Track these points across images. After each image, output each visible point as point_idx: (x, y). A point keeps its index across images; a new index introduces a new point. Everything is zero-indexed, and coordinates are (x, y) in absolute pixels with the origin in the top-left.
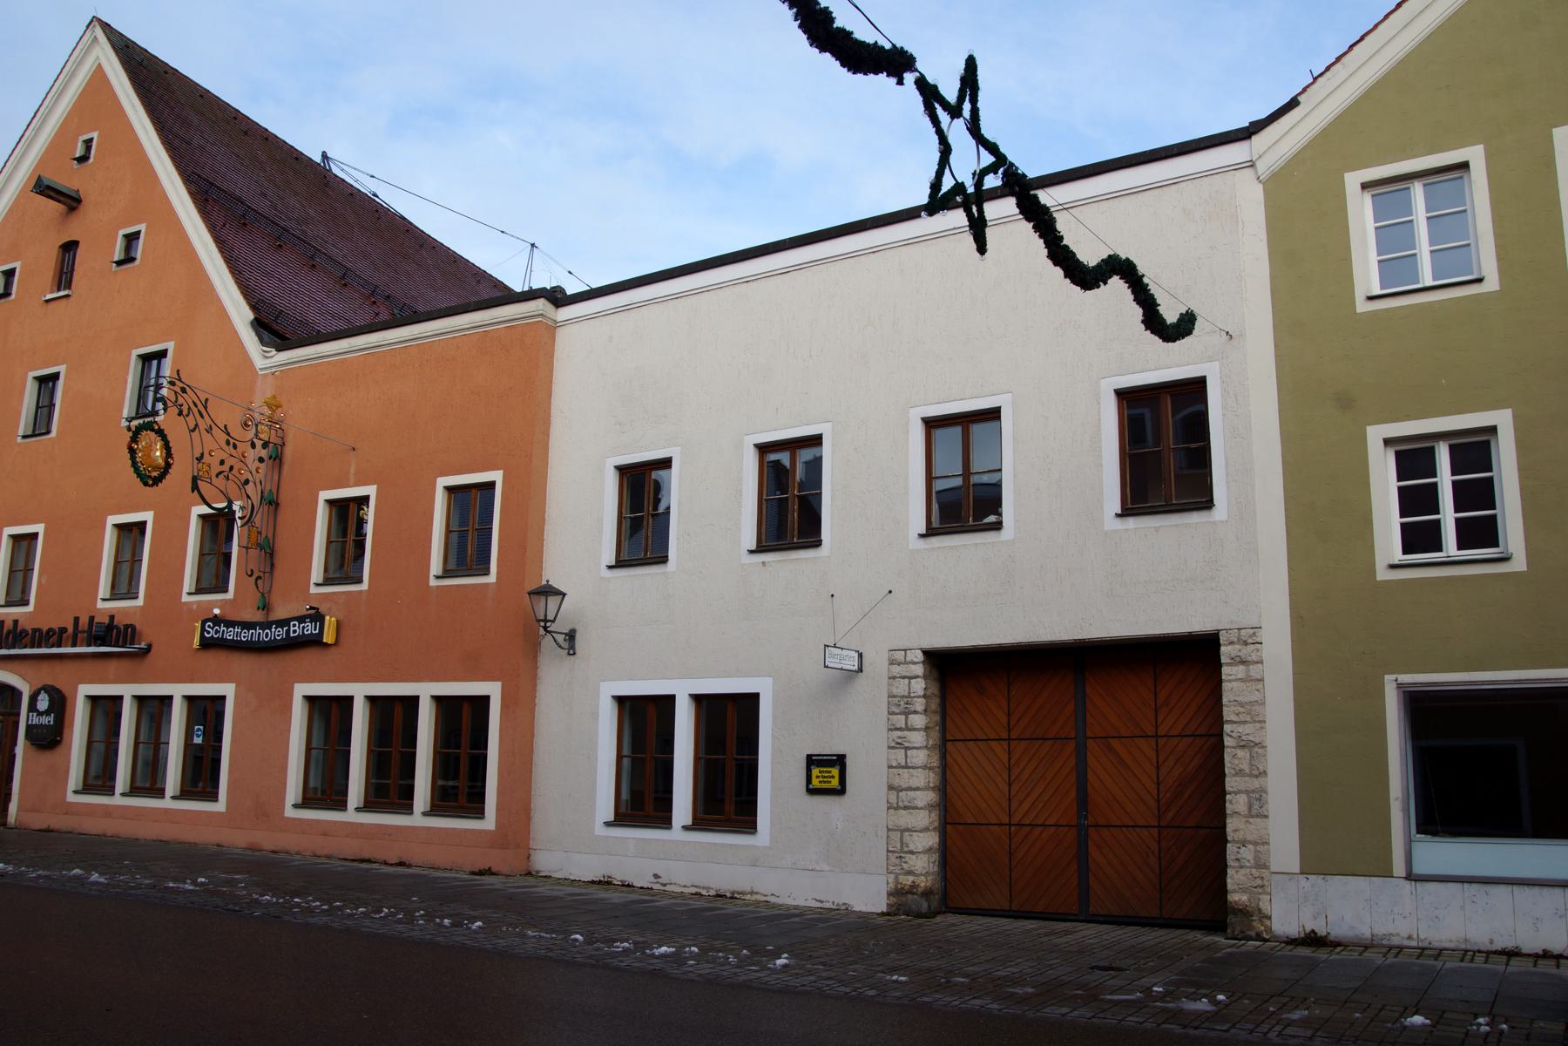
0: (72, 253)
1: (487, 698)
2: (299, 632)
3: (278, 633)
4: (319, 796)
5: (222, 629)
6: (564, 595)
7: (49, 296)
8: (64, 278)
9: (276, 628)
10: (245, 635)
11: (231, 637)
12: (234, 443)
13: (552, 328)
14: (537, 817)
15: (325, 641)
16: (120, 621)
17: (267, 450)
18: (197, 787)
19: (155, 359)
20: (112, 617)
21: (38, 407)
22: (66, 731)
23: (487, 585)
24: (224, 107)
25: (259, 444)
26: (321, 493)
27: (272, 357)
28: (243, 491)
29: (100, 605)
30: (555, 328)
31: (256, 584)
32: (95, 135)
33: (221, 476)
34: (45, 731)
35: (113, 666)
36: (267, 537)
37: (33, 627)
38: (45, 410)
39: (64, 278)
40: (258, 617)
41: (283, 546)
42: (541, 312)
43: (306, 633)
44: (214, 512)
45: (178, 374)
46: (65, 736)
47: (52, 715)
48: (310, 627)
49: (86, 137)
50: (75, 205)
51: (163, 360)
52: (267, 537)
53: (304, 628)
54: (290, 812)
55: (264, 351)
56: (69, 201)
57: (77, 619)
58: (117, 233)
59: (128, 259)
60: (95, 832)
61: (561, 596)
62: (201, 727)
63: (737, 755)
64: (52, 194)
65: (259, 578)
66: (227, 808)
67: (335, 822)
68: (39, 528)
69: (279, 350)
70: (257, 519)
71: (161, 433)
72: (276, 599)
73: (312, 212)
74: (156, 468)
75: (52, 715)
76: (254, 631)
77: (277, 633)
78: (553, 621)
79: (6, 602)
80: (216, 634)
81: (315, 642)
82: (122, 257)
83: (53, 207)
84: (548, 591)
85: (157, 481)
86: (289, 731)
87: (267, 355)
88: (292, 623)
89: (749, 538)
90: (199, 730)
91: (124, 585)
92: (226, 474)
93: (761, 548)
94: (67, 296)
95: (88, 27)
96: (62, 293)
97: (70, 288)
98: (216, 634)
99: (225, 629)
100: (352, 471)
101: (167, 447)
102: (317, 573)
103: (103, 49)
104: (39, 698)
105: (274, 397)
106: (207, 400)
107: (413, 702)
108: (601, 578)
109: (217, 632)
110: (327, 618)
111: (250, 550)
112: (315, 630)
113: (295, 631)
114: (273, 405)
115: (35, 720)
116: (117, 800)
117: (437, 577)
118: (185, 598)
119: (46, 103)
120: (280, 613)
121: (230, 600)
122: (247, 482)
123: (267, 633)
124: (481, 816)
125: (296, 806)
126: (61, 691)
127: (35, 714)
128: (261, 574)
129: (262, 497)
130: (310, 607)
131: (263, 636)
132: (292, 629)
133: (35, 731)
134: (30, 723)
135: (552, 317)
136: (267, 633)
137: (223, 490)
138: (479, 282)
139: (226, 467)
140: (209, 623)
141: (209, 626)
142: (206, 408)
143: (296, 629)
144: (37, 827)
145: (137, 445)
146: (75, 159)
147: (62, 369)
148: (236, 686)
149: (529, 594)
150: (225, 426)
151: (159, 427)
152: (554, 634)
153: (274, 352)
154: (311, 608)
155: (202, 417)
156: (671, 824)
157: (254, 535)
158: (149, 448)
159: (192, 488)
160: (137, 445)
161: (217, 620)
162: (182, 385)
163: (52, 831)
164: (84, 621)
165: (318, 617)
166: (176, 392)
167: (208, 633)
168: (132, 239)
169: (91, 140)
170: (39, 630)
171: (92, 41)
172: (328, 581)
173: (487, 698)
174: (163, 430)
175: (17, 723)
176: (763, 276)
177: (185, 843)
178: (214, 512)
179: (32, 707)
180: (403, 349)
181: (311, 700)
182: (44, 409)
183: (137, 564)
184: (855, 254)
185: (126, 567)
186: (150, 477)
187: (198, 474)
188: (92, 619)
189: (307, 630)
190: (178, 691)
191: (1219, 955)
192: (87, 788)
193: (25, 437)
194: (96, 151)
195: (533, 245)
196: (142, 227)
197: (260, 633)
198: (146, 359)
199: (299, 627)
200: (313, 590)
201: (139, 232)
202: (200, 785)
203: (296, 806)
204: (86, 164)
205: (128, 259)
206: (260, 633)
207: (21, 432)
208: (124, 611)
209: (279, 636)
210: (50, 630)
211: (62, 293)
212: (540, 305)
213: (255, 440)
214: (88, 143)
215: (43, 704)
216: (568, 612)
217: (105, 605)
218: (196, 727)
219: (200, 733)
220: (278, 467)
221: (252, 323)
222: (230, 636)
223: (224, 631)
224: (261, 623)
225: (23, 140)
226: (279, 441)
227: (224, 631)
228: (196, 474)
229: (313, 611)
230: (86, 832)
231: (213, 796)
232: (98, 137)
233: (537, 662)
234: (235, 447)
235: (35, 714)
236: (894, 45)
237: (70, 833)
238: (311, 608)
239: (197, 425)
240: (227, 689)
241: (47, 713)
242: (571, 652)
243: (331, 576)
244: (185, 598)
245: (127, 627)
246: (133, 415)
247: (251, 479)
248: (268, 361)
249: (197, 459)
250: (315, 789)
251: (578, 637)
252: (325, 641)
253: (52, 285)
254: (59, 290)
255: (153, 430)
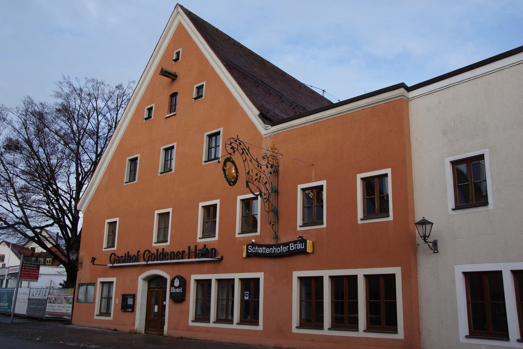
0: (174, 98)
1: (259, 279)
2: (294, 248)
3: (285, 249)
4: (305, 322)
5: (256, 248)
6: (432, 224)
7: (167, 116)
8: (172, 107)
9: (283, 247)
10: (268, 251)
11: (261, 252)
12: (260, 166)
13: (408, 100)
14: (424, 333)
15: (307, 251)
16: (209, 247)
17: (272, 168)
18: (247, 319)
19: (169, 150)
20: (205, 245)
21: (130, 171)
22: (187, 295)
23: (323, 228)
24: (225, 35)
25: (269, 166)
26: (200, 203)
27: (269, 129)
28: (265, 187)
29: (154, 245)
30: (408, 101)
31: (272, 228)
32: (181, 50)
33: (256, 181)
34: (178, 295)
35: (206, 267)
36: (275, 207)
37: (211, 248)
38: (133, 172)
39: (172, 107)
40: (273, 242)
41: (283, 209)
42: (403, 94)
43: (298, 248)
44: (255, 196)
45: (238, 137)
46: (186, 297)
47: (181, 288)
48: (299, 246)
49: (177, 51)
50: (175, 78)
51: (173, 150)
52: (275, 207)
53: (296, 246)
54: (294, 330)
55: (266, 127)
56: (173, 77)
57: (189, 247)
58: (194, 87)
59: (199, 96)
60: (202, 339)
61: (431, 224)
62: (248, 292)
63: (385, 300)
64: (167, 74)
65: (273, 225)
66: (263, 328)
67: (318, 335)
68: (170, 210)
69: (272, 126)
70: (271, 199)
71: (233, 162)
72: (280, 234)
73: (263, 74)
74: (233, 177)
75: (181, 288)
76: (272, 249)
77: (283, 249)
78: (428, 237)
79: (158, 241)
80: (254, 251)
81: (303, 252)
82: (196, 96)
83: (167, 80)
84: (424, 222)
85: (234, 183)
86: (292, 293)
88: (290, 244)
89: (451, 203)
90: (247, 293)
91: (209, 231)
92: (258, 179)
93: (457, 208)
94: (175, 115)
95: (175, 8)
96: (172, 114)
97: (175, 111)
98: (254, 251)
100: (313, 174)
101: (236, 169)
102: (300, 222)
103: (181, 16)
104: (175, 281)
105: (274, 146)
106: (249, 148)
107: (354, 278)
108: (449, 215)
110: (308, 241)
111: (269, 213)
112: (302, 247)
113: (292, 248)
114: (273, 149)
115: (174, 290)
116: (211, 325)
117: (300, 226)
118: (237, 236)
119: (161, 40)
120: (283, 240)
121: (258, 236)
122: (266, 183)
123: (279, 249)
124: (396, 332)
125: (297, 327)
126: (184, 278)
127: (174, 288)
128: (274, 223)
129: (272, 189)
130: (299, 236)
131: (276, 251)
133: (174, 295)
134: (172, 292)
135: (407, 96)
136: (279, 249)
137: (258, 186)
138: (323, 101)
139: (258, 177)
140: (250, 246)
141: (250, 247)
142: (249, 151)
143: (292, 247)
144: (176, 336)
145: (226, 168)
146: (173, 60)
147: (175, 144)
149: (415, 224)
150: (256, 159)
151: (233, 160)
152: (429, 243)
153: (270, 127)
154: (299, 237)
155: (248, 155)
156: (397, 331)
157: (270, 206)
158: (230, 169)
159: (247, 186)
160: (226, 168)
161: (253, 245)
162: (239, 142)
163: (183, 338)
164: (193, 248)
165: (303, 241)
166: (237, 145)
167: (250, 250)
168: (200, 88)
169: (179, 52)
170: (174, 252)
171: (177, 13)
172: (304, 225)
173: (259, 279)
174: (234, 161)
175: (165, 292)
176: (467, 80)
177: (244, 344)
178: (255, 196)
179: (172, 284)
180: (303, 129)
181: (300, 278)
182: (167, 161)
184: (489, 73)
185: (162, 230)
186: (231, 181)
187: (248, 180)
188: (196, 247)
190: (237, 276)
192: (197, 319)
193: (161, 173)
194: (181, 56)
195: (324, 91)
196: (204, 83)
198: (166, 150)
199: (294, 246)
200: (299, 229)
201: (203, 85)
202: (249, 318)
203: (192, 321)
204: (178, 61)
205: (149, 117)
206: (275, 250)
207: (160, 171)
208: (210, 243)
209: (284, 250)
210: (178, 252)
211: (172, 114)
212: (402, 90)
213: (268, 164)
214: (178, 54)
215: (177, 283)
216: (435, 232)
217: (155, 245)
218: (245, 292)
219: (247, 295)
220: (277, 175)
221: (259, 116)
222: (260, 251)
223: (257, 249)
224: (276, 245)
225: (153, 56)
226: (276, 165)
227: (257, 249)
228: (247, 180)
229: (300, 239)
230: (198, 339)
231: (256, 322)
232: (182, 50)
233: (416, 257)
234: (261, 168)
235: (174, 288)
237: (191, 339)
238: (299, 237)
239: (246, 159)
240: (260, 275)
241: (179, 287)
242: (436, 251)
243: (244, 230)
244: (237, 236)
245: (212, 249)
247: (268, 181)
248: (268, 131)
249: (247, 173)
250: (304, 319)
251: (439, 244)
252: (307, 251)
253: (168, 111)
254: (170, 113)
255: (230, 161)
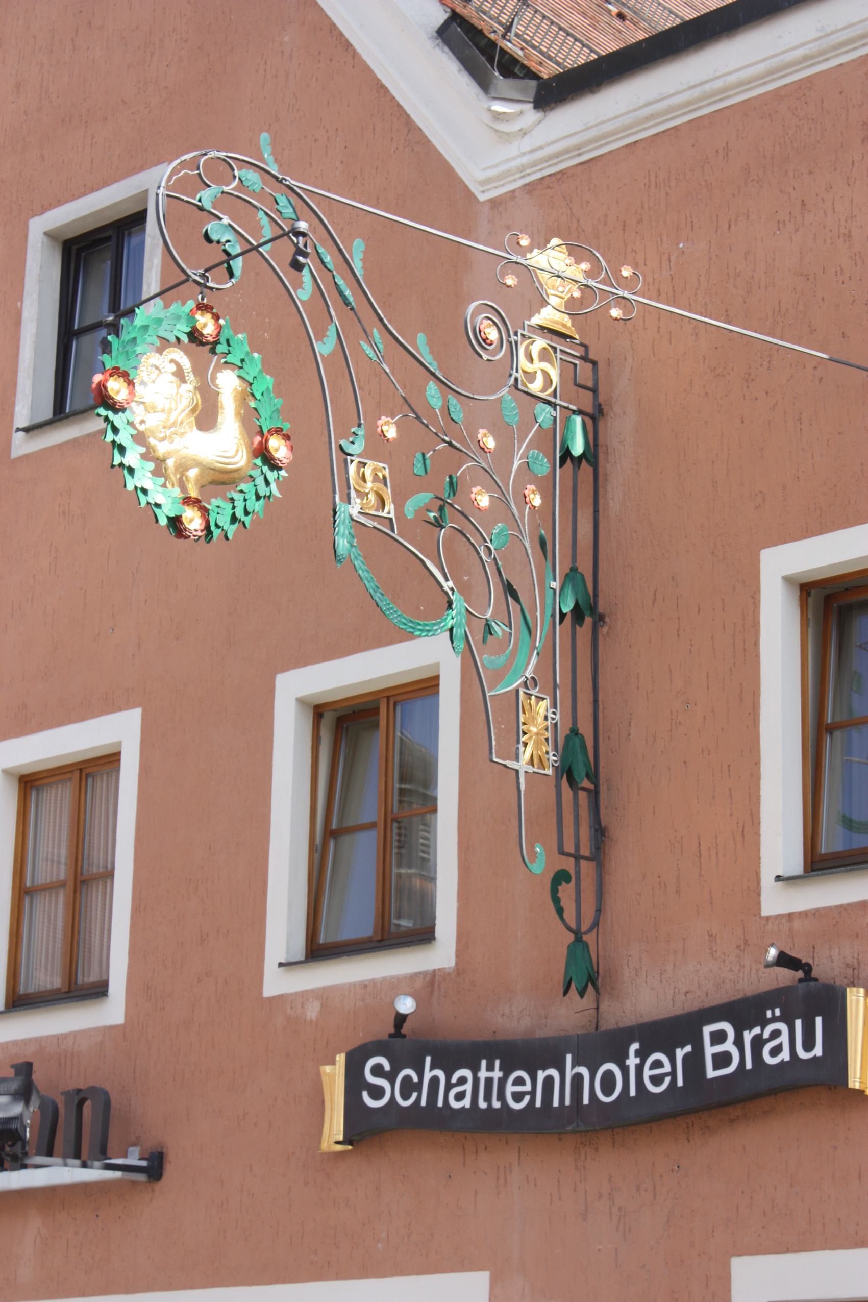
5: (428, 1075)
9: (642, 1054)
11: (466, 1103)
31: (556, 900)
48: (784, 1039)
53: (758, 1043)
76: (553, 1072)
87: (503, 127)
88: (707, 1030)
99: (440, 1073)
109: (408, 1087)
112: (809, 1045)
113: (722, 1060)
128: (569, 864)
132: (710, 1050)
141: (378, 1071)
148: (494, 1282)
167: (377, 1093)
183: (95, 895)
189: (775, 1051)
191: (213, 387)
197: (578, 1078)
199: (739, 1042)
206: (578, 1078)
209: (656, 1080)
222: (460, 1097)
223: (435, 1081)
227: (435, 1081)
236: (681, 18)
238: (784, 960)
245: (79, 1098)
246: (47, 412)
248: (513, 149)
249: (568, 881)
